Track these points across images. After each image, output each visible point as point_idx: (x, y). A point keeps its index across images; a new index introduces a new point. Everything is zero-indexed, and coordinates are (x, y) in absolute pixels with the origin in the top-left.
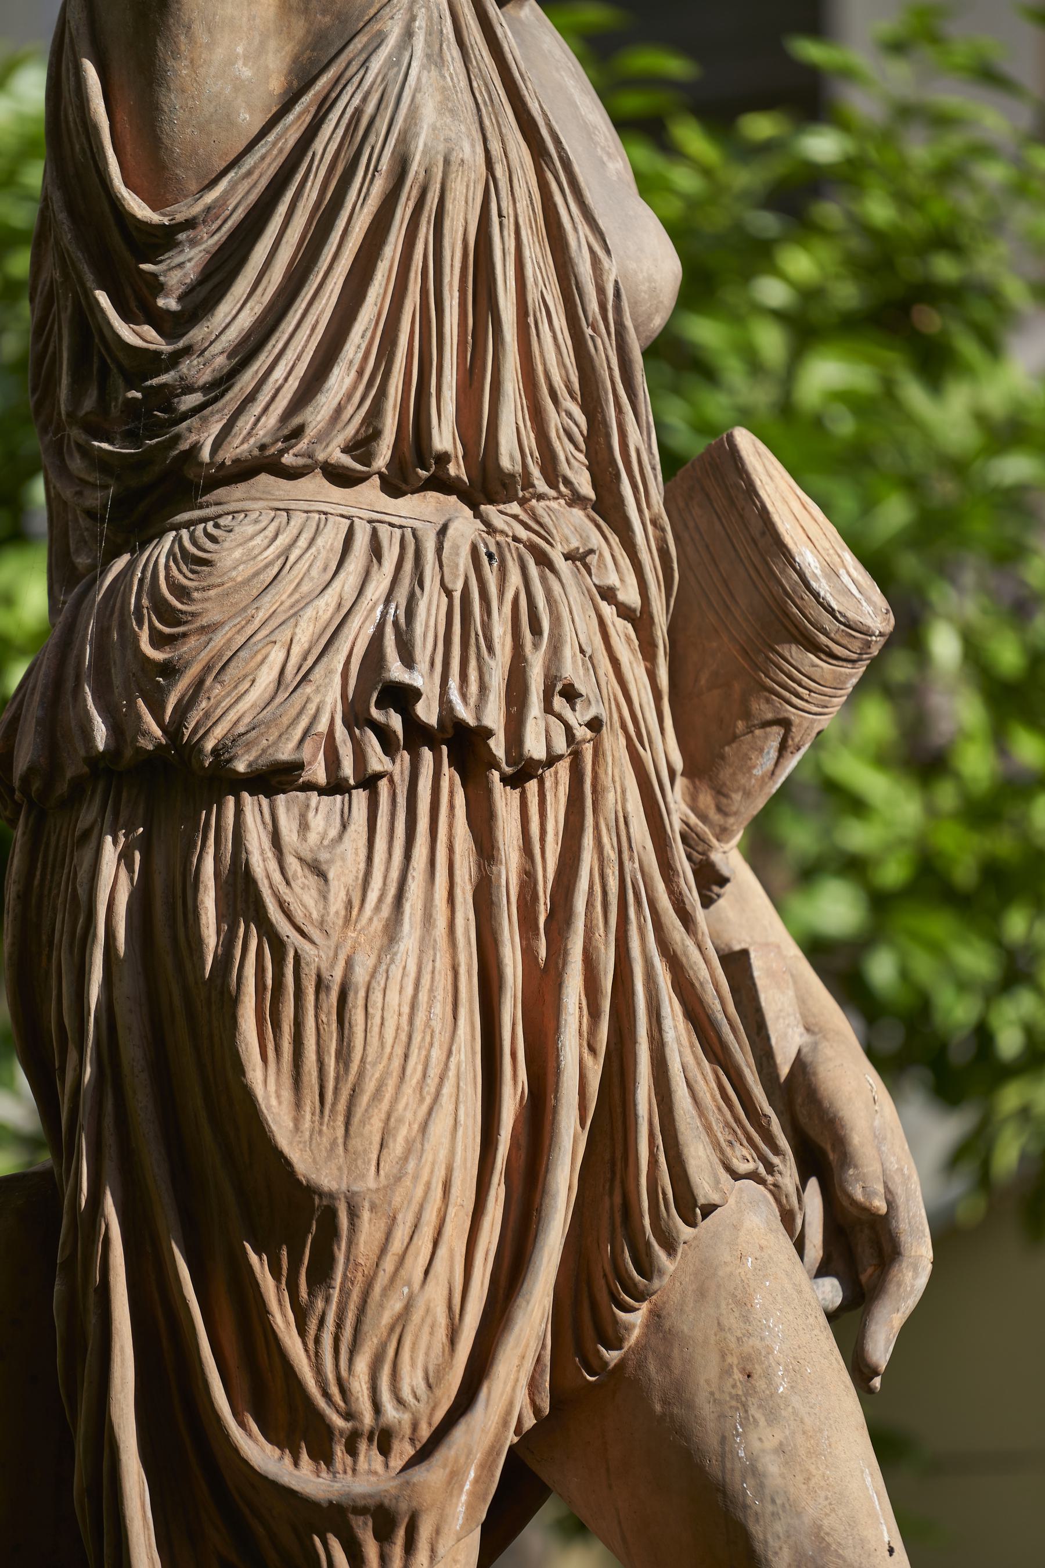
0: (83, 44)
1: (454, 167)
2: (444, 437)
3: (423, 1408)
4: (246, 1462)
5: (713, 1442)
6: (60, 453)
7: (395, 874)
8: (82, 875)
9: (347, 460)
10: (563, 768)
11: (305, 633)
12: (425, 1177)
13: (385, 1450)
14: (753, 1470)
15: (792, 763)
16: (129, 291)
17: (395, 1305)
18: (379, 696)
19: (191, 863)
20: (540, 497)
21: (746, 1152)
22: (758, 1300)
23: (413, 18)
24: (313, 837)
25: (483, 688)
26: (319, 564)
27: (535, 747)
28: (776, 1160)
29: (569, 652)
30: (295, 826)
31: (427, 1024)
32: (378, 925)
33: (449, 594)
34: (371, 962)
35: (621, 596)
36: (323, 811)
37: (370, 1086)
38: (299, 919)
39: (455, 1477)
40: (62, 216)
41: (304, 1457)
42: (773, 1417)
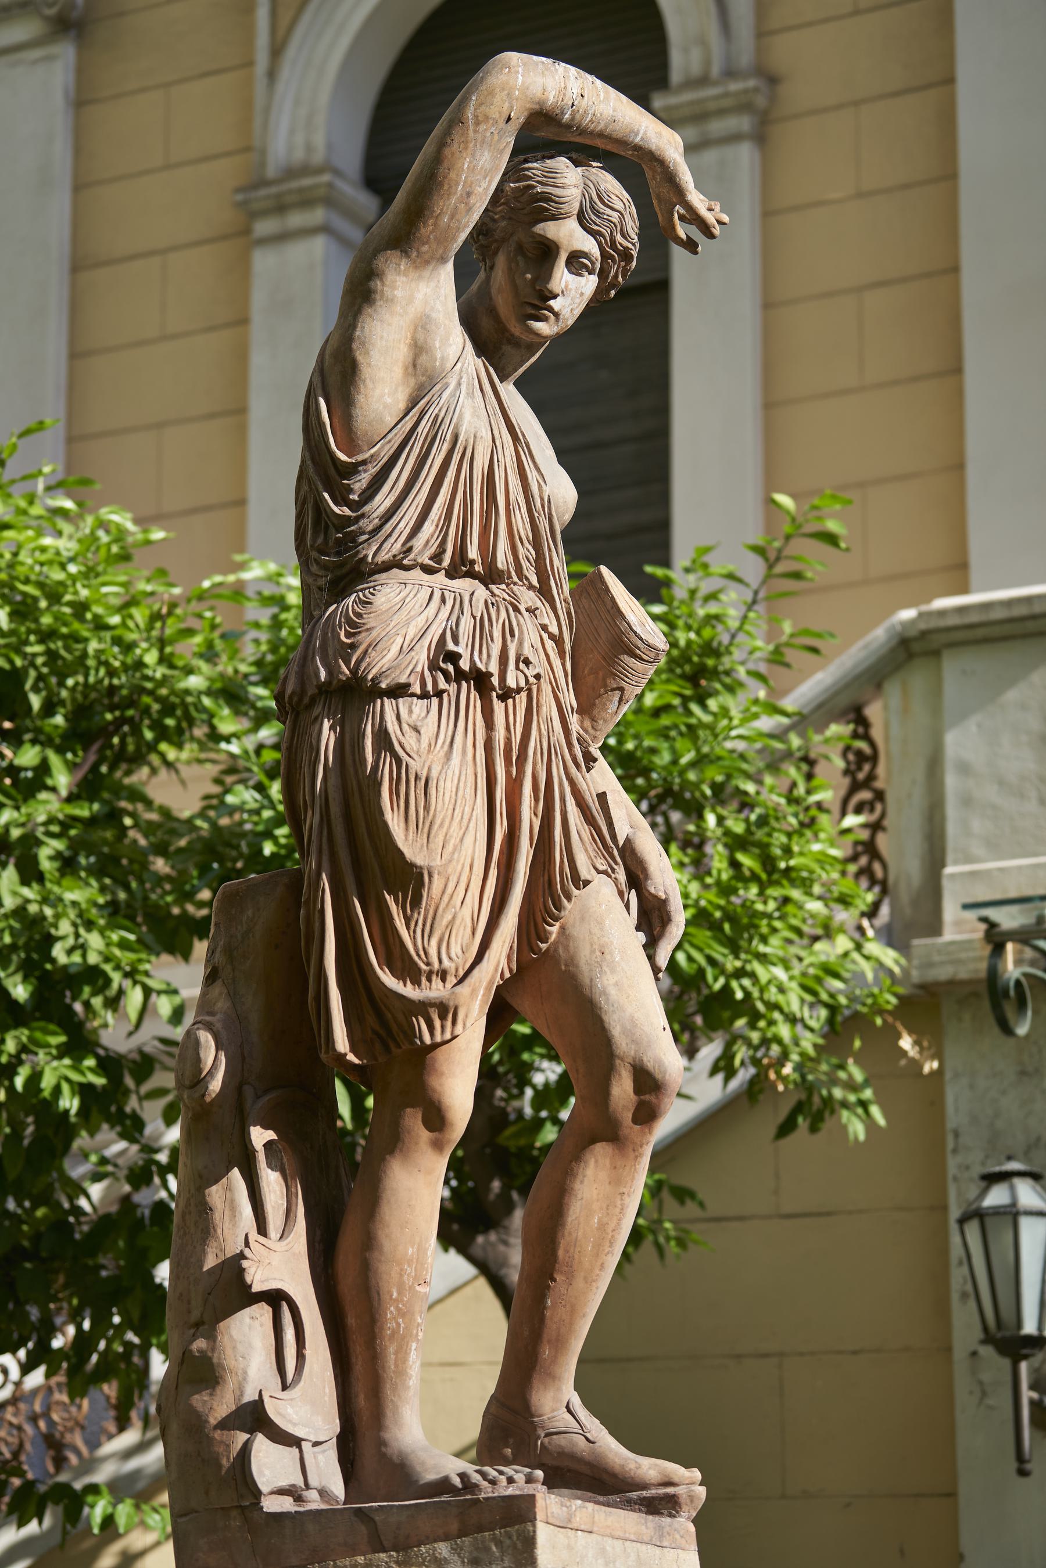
0: (319, 391)
1: (478, 439)
2: (473, 553)
3: (460, 961)
4: (383, 984)
5: (587, 981)
6: (308, 565)
7: (450, 733)
8: (315, 735)
9: (431, 563)
10: (524, 694)
11: (412, 632)
12: (462, 862)
13: (444, 980)
14: (604, 992)
15: (625, 708)
16: (337, 493)
17: (448, 917)
18: (444, 657)
19: (364, 760)
20: (515, 584)
21: (603, 861)
22: (607, 922)
23: (461, 378)
24: (414, 716)
25: (489, 656)
26: (418, 605)
27: (511, 682)
28: (615, 867)
29: (526, 645)
30: (407, 711)
31: (464, 796)
32: (442, 754)
33: (475, 618)
34: (439, 768)
35: (550, 629)
36: (419, 706)
37: (438, 822)
38: (408, 749)
39: (474, 992)
40: (309, 462)
41: (408, 982)
42: (613, 971)
